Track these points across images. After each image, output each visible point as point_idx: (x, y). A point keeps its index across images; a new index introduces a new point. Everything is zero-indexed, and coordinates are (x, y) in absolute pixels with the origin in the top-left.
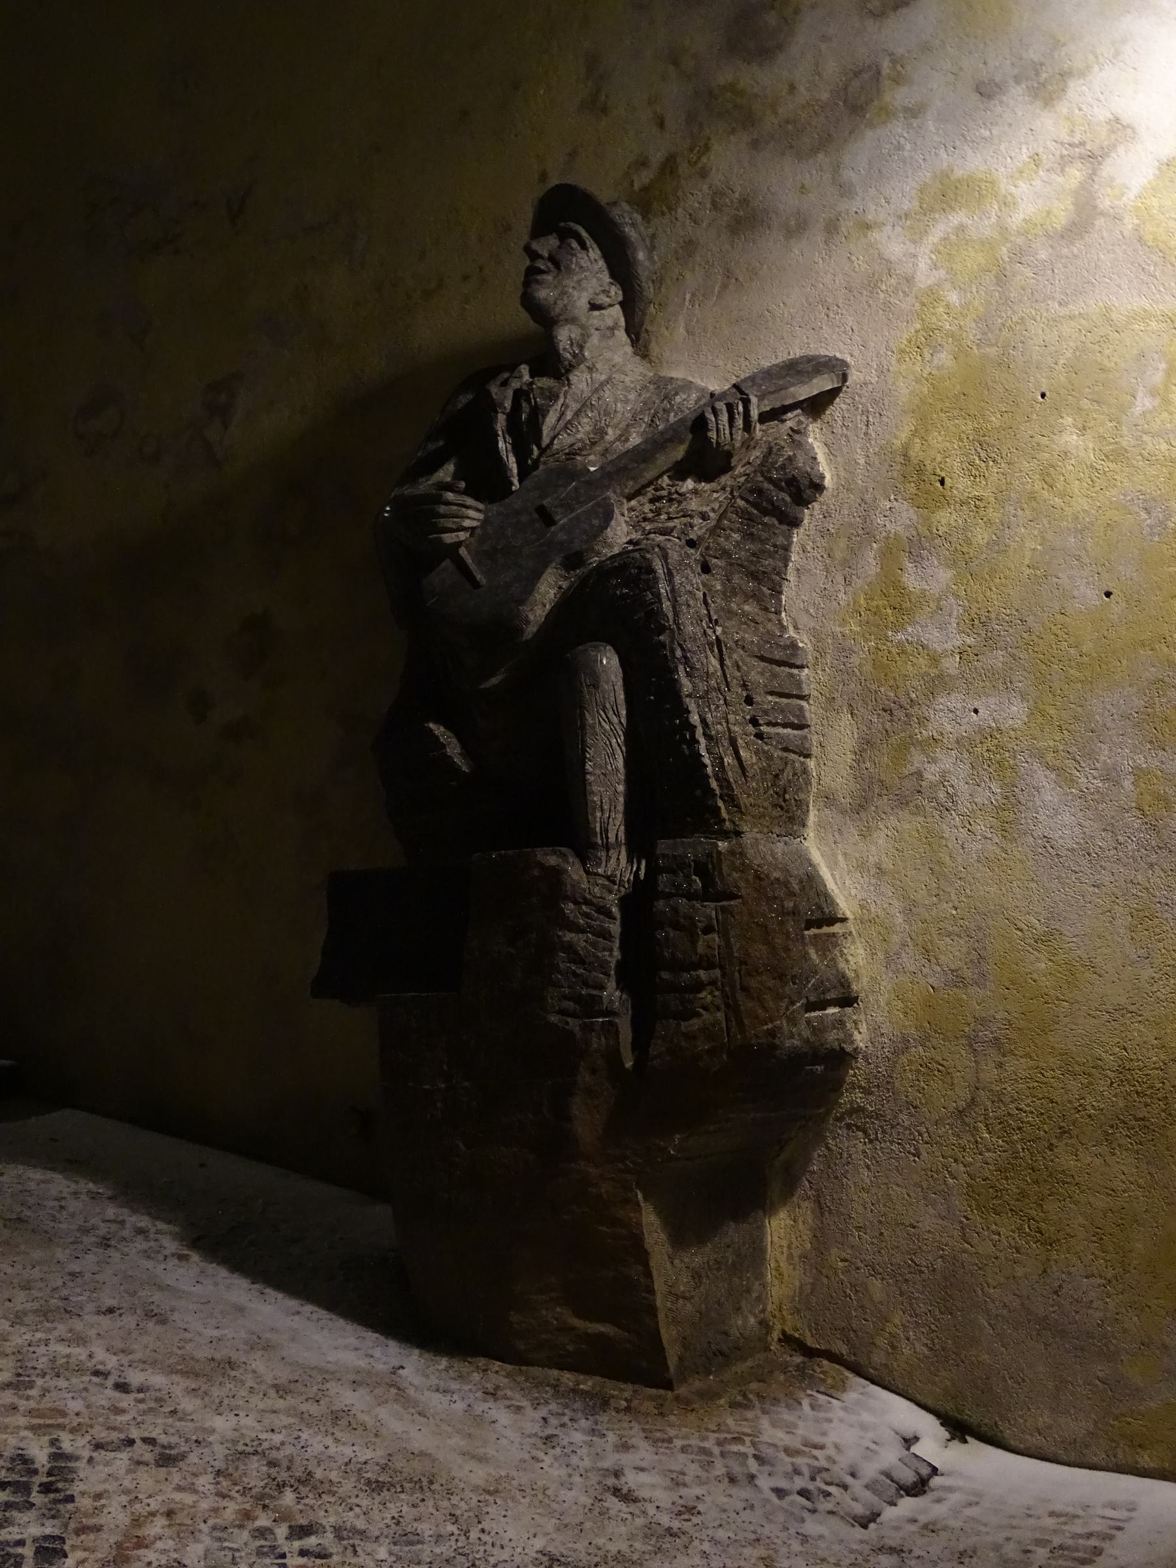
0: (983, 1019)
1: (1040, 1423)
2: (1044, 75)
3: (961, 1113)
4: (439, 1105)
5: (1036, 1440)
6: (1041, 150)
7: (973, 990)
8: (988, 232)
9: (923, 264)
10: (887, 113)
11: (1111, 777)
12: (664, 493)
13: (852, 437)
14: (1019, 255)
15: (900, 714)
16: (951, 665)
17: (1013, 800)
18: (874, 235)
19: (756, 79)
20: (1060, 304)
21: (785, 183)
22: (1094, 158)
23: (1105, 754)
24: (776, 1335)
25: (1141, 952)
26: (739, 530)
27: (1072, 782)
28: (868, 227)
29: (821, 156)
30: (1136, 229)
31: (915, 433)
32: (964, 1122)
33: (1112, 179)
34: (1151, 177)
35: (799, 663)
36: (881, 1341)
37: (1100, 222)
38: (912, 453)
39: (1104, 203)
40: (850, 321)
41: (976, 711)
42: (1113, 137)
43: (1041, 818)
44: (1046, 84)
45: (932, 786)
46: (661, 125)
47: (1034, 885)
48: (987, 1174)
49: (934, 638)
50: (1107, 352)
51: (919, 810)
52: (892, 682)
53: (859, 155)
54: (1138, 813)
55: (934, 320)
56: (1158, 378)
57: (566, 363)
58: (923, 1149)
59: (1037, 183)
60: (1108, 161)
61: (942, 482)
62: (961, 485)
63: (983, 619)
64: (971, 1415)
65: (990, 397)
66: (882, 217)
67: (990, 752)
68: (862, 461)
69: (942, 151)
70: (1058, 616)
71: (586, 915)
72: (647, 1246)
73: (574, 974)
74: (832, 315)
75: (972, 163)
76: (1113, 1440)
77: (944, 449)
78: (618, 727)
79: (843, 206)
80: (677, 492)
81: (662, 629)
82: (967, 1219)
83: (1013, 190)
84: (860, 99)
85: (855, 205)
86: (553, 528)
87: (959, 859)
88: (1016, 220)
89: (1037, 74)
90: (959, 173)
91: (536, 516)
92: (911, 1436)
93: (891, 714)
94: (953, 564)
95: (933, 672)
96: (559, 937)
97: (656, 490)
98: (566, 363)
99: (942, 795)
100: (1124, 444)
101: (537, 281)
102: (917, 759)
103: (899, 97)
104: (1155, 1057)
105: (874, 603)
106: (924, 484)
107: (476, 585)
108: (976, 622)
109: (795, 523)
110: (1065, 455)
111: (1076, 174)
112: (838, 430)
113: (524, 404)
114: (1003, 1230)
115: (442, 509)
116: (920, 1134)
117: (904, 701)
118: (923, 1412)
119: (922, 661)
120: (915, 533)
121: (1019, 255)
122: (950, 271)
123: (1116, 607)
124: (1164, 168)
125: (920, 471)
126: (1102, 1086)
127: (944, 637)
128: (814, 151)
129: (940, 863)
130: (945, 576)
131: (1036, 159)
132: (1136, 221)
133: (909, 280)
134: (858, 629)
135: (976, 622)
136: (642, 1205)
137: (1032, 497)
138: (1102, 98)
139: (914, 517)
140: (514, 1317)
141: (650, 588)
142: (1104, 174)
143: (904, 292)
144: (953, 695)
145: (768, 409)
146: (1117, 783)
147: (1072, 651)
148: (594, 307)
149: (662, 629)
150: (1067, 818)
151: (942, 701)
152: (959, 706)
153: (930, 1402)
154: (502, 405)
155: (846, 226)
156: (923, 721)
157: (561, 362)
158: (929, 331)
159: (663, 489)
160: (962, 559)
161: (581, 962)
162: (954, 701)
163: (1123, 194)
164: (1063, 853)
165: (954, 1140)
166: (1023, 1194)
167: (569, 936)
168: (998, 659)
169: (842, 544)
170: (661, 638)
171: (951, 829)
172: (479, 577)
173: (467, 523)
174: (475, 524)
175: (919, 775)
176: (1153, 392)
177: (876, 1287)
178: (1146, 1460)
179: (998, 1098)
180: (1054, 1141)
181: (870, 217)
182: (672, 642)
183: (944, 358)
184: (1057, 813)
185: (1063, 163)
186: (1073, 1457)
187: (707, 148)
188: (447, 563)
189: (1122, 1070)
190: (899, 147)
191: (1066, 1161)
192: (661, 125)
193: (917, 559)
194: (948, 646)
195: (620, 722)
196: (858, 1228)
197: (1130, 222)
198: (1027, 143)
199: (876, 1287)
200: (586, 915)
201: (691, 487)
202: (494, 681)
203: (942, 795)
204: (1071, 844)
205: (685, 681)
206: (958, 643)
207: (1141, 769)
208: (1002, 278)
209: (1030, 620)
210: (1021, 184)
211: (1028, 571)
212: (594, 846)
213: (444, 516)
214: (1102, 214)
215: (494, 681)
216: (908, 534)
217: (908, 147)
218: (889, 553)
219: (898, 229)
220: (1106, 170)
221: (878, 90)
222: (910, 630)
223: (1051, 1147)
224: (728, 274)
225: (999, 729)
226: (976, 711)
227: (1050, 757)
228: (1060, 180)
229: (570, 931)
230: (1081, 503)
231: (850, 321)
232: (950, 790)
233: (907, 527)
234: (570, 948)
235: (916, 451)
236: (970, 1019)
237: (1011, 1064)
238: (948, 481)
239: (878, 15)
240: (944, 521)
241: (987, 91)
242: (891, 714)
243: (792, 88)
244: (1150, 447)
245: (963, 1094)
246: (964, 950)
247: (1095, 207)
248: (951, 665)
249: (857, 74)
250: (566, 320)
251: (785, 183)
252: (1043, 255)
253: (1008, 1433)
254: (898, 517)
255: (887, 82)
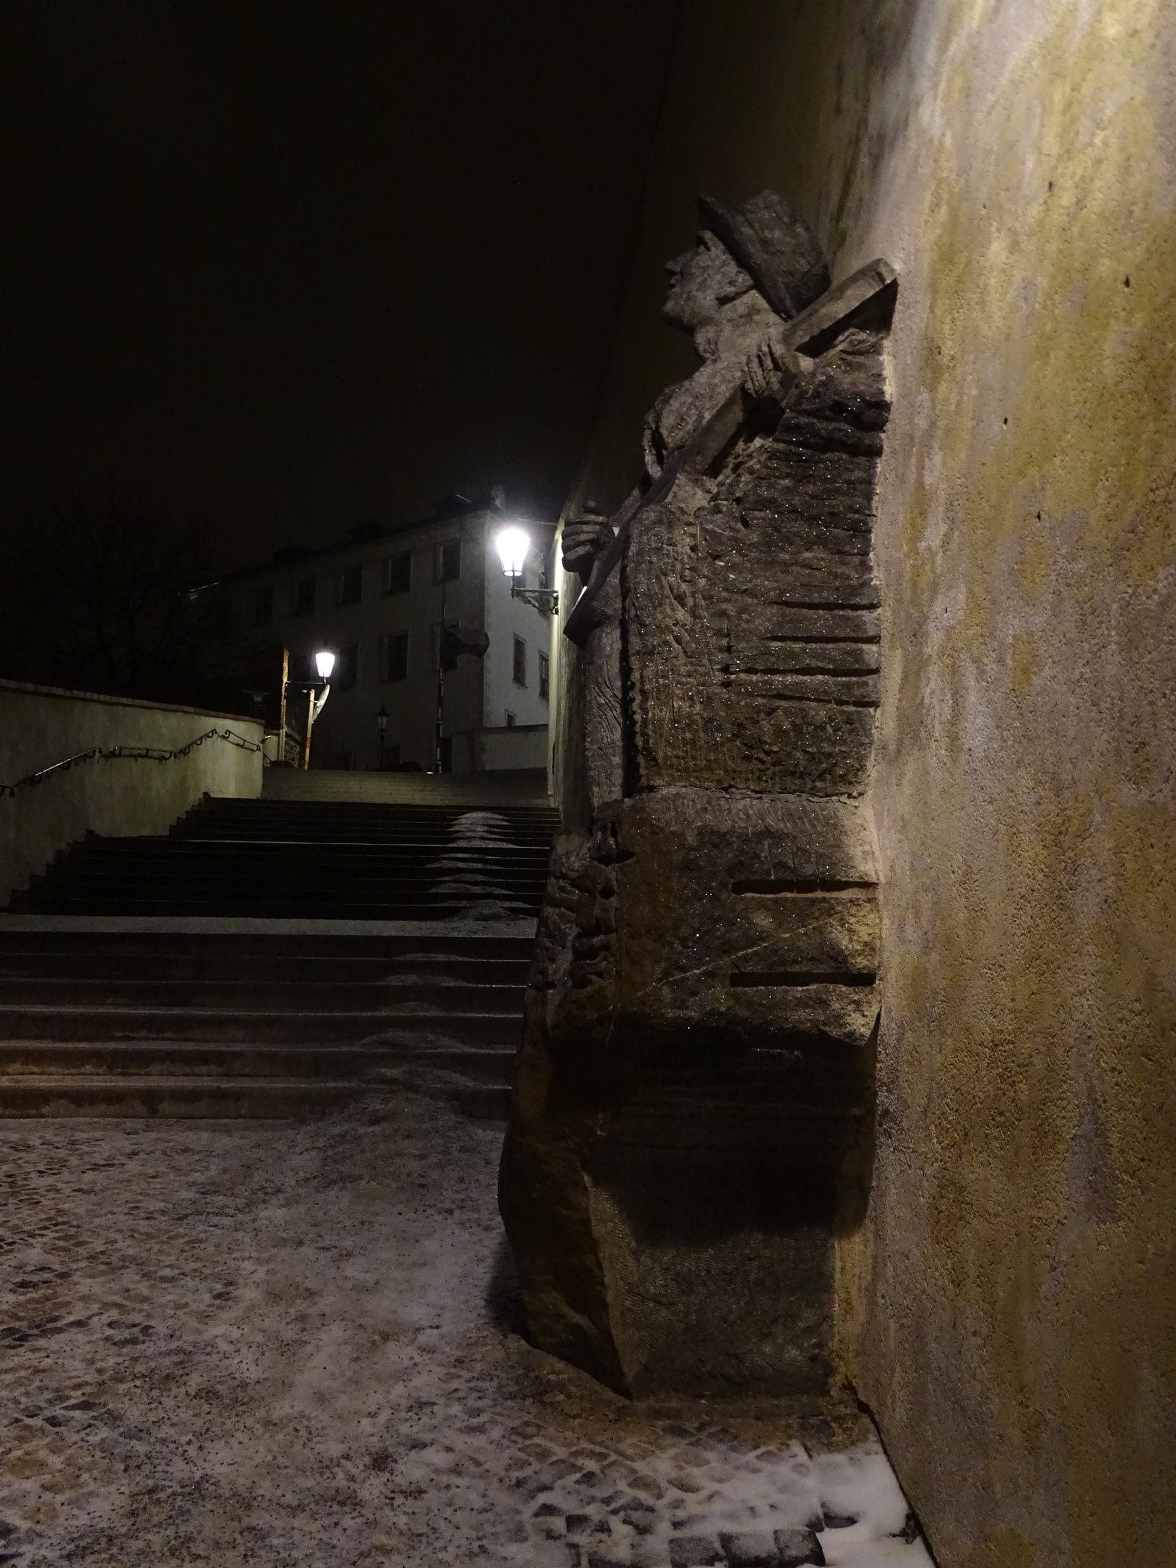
24: (839, 1379)
26: (788, 476)
35: (865, 602)
72: (596, 1234)
78: (612, 699)
92: (846, 1514)
97: (736, 458)
109: (876, 451)
118: (901, 1495)
136: (591, 1189)
145: (807, 339)
148: (723, 301)
173: (583, 537)
174: (591, 536)
195: (615, 695)
200: (562, 889)
201: (758, 445)
250: (700, 323)
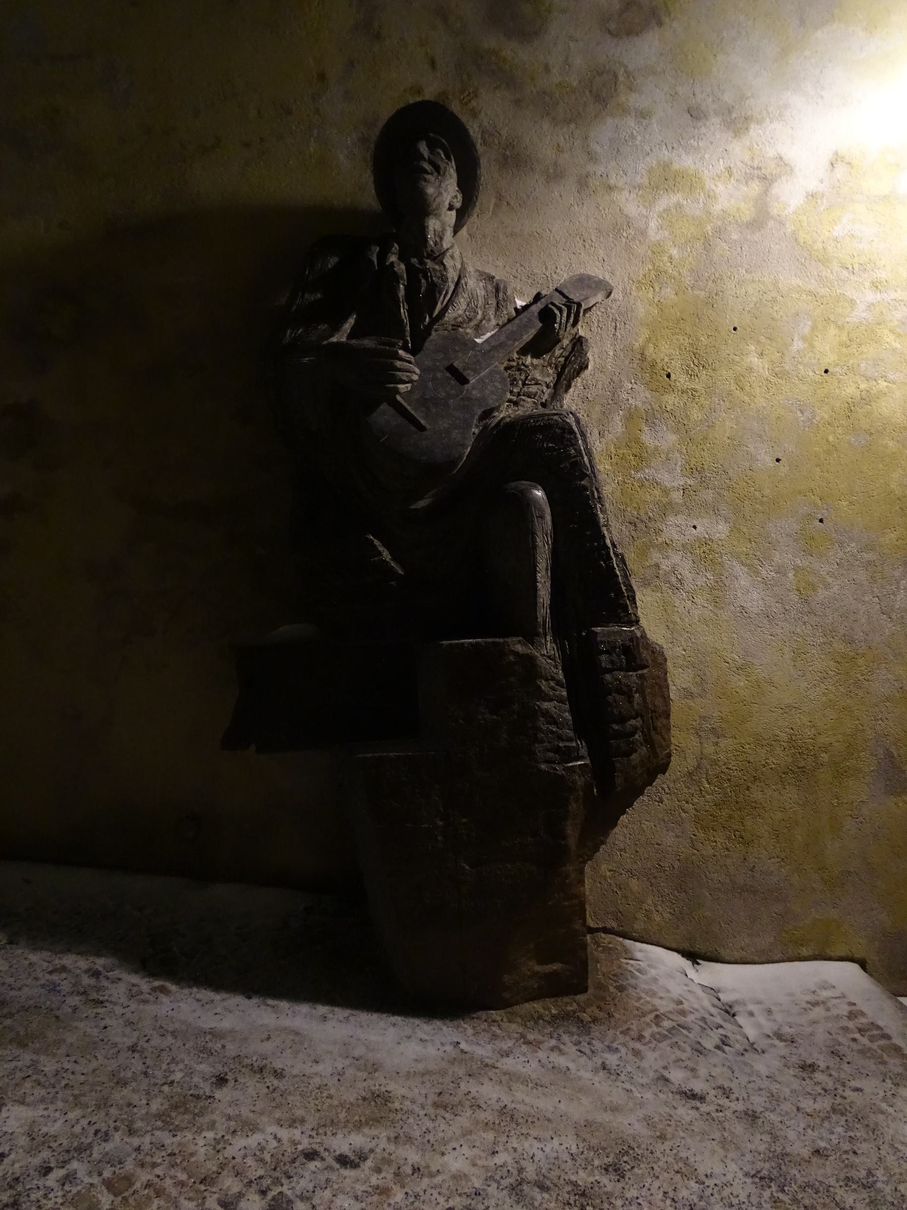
0: (704, 717)
1: (743, 944)
2: (734, 115)
3: (690, 774)
4: (440, 838)
5: (737, 955)
6: (732, 165)
7: (699, 700)
8: (698, 213)
9: (653, 224)
10: (625, 111)
11: (781, 571)
12: (514, 364)
13: (604, 335)
14: (719, 232)
15: (640, 526)
16: (677, 497)
17: (721, 584)
18: (615, 195)
19: (515, 53)
20: (746, 271)
21: (544, 140)
22: (768, 181)
23: (777, 558)
25: (799, 673)
27: (757, 573)
28: (610, 188)
29: (573, 126)
30: (794, 232)
31: (649, 340)
32: (692, 779)
33: (778, 198)
34: (802, 202)
36: (640, 916)
37: (771, 223)
38: (646, 353)
39: (774, 212)
40: (601, 253)
41: (695, 527)
42: (779, 169)
43: (739, 595)
44: (737, 122)
45: (666, 574)
46: (433, 64)
47: (735, 636)
48: (707, 808)
49: (665, 478)
50: (775, 308)
51: (657, 589)
52: (635, 505)
53: (603, 133)
54: (797, 593)
55: (661, 264)
56: (807, 331)
57: (429, 249)
58: (664, 797)
59: (730, 186)
60: (776, 184)
61: (669, 376)
62: (681, 380)
63: (699, 469)
64: (700, 947)
65: (703, 327)
66: (620, 184)
67: (705, 554)
68: (611, 353)
69: (664, 147)
70: (748, 471)
71: (553, 689)
73: (552, 732)
74: (587, 246)
75: (686, 162)
76: (785, 945)
77: (666, 352)
79: (591, 168)
80: (524, 365)
81: (584, 476)
82: (695, 835)
83: (713, 187)
84: (601, 92)
85: (600, 170)
86: (466, 386)
87: (687, 620)
88: (717, 208)
89: (730, 112)
90: (676, 166)
91: (448, 375)
93: (635, 526)
94: (677, 431)
95: (664, 500)
96: (538, 706)
98: (429, 249)
99: (673, 580)
100: (787, 368)
101: (425, 180)
102: (655, 556)
103: (634, 100)
104: (810, 732)
105: (622, 451)
106: (658, 377)
107: (422, 428)
108: (694, 470)
110: (750, 369)
111: (755, 187)
112: (594, 329)
113: (423, 281)
114: (717, 839)
115: (398, 364)
116: (663, 789)
117: (644, 518)
119: (657, 492)
120: (649, 407)
121: (719, 232)
122: (671, 233)
123: (783, 468)
124: (810, 198)
125: (653, 365)
126: (778, 751)
127: (672, 479)
128: (568, 122)
129: (675, 623)
130: (672, 438)
131: (729, 170)
132: (793, 228)
133: (643, 233)
134: (610, 467)
135: (694, 470)
137: (730, 394)
138: (772, 142)
139: (649, 396)
140: (506, 978)
141: (572, 445)
142: (773, 192)
143: (640, 241)
144: (679, 516)
146: (785, 575)
147: (757, 493)
149: (584, 476)
150: (755, 596)
151: (671, 519)
152: (683, 523)
153: (674, 946)
154: (402, 278)
155: (593, 183)
156: (659, 532)
157: (426, 247)
158: (659, 272)
159: (514, 360)
160: (682, 427)
161: (555, 723)
162: (680, 520)
163: (785, 208)
164: (753, 616)
165: (685, 790)
166: (731, 817)
167: (546, 705)
168: (708, 495)
169: (598, 408)
170: (583, 482)
171: (679, 601)
172: (423, 422)
175: (657, 566)
176: (804, 339)
177: (634, 884)
178: (805, 952)
179: (715, 763)
180: (749, 784)
181: (612, 182)
182: (592, 487)
183: (669, 293)
184: (748, 591)
185: (748, 178)
186: (764, 959)
187: (476, 95)
188: (384, 406)
189: (791, 740)
190: (633, 137)
191: (757, 795)
192: (433, 64)
193: (652, 425)
194: (675, 484)
196: (621, 850)
197: (790, 227)
198: (723, 158)
199: (634, 884)
200: (553, 689)
202: (422, 504)
203: (673, 580)
204: (756, 610)
205: (601, 516)
206: (682, 483)
207: (798, 567)
208: (707, 244)
209: (731, 472)
210: (719, 184)
211: (729, 441)
212: (538, 635)
213: (400, 370)
214: (772, 218)
215: (422, 504)
216: (644, 407)
217: (639, 138)
218: (631, 417)
219: (633, 196)
220: (775, 190)
221: (616, 90)
222: (647, 471)
223: (748, 789)
224: (500, 198)
225: (710, 539)
226: (695, 527)
227: (743, 557)
228: (745, 189)
229: (544, 701)
230: (761, 402)
231: (601, 253)
232: (679, 577)
233: (644, 403)
234: (546, 714)
235: (650, 350)
236: (697, 718)
237: (723, 743)
238: (673, 376)
239: (615, 35)
240: (670, 402)
241: (695, 114)
242: (635, 526)
243: (547, 69)
244: (802, 372)
245: (692, 763)
246: (692, 676)
247: (768, 213)
248: (677, 497)
249: (600, 74)
251: (544, 140)
252: (735, 236)
253: (723, 953)
254: (639, 396)
255: (622, 87)
